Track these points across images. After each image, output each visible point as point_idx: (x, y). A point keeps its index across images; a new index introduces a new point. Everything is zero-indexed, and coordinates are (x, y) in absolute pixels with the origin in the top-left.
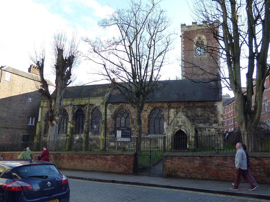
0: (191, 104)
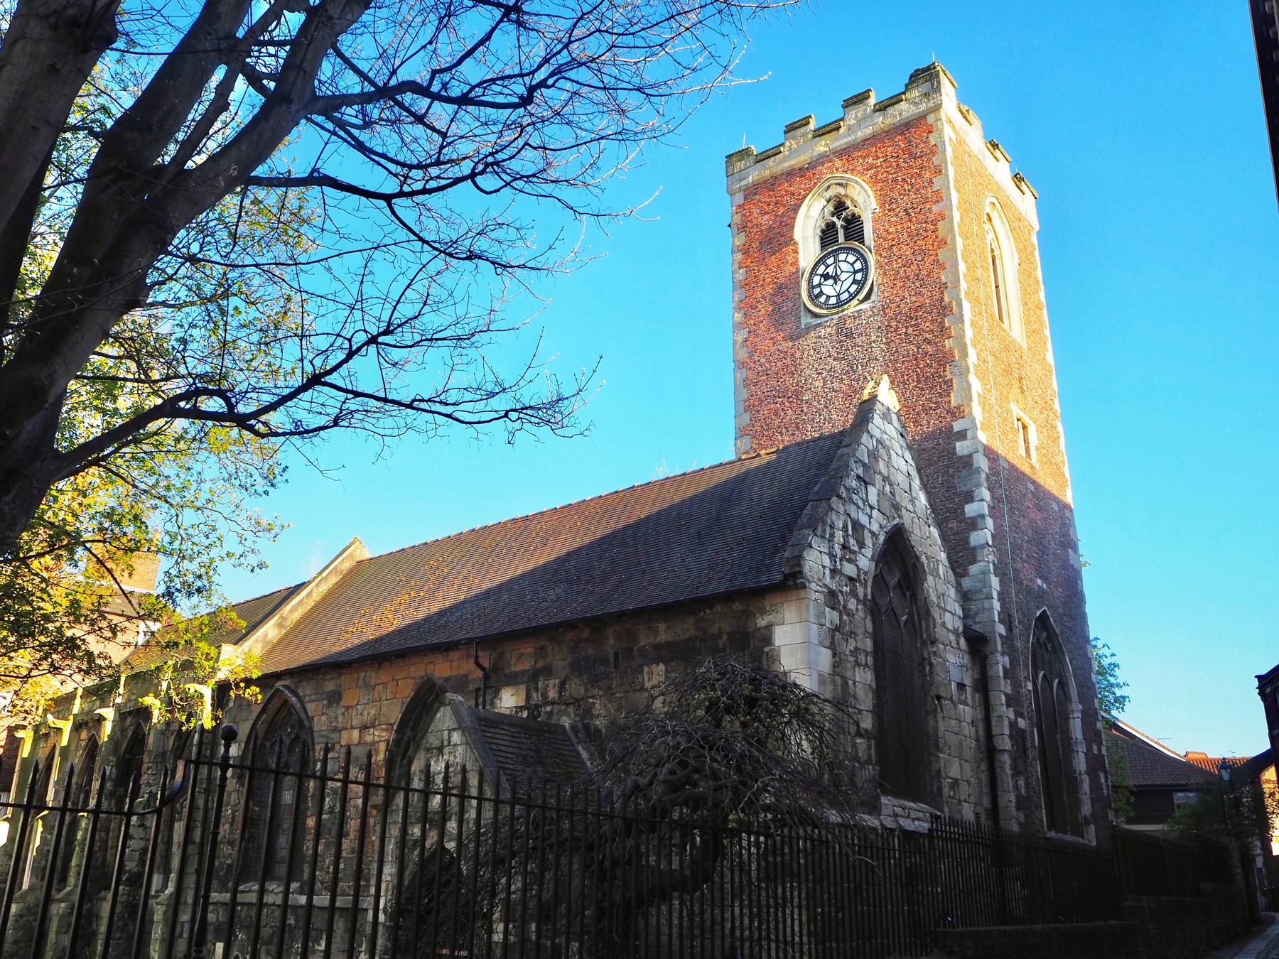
0: (612, 641)
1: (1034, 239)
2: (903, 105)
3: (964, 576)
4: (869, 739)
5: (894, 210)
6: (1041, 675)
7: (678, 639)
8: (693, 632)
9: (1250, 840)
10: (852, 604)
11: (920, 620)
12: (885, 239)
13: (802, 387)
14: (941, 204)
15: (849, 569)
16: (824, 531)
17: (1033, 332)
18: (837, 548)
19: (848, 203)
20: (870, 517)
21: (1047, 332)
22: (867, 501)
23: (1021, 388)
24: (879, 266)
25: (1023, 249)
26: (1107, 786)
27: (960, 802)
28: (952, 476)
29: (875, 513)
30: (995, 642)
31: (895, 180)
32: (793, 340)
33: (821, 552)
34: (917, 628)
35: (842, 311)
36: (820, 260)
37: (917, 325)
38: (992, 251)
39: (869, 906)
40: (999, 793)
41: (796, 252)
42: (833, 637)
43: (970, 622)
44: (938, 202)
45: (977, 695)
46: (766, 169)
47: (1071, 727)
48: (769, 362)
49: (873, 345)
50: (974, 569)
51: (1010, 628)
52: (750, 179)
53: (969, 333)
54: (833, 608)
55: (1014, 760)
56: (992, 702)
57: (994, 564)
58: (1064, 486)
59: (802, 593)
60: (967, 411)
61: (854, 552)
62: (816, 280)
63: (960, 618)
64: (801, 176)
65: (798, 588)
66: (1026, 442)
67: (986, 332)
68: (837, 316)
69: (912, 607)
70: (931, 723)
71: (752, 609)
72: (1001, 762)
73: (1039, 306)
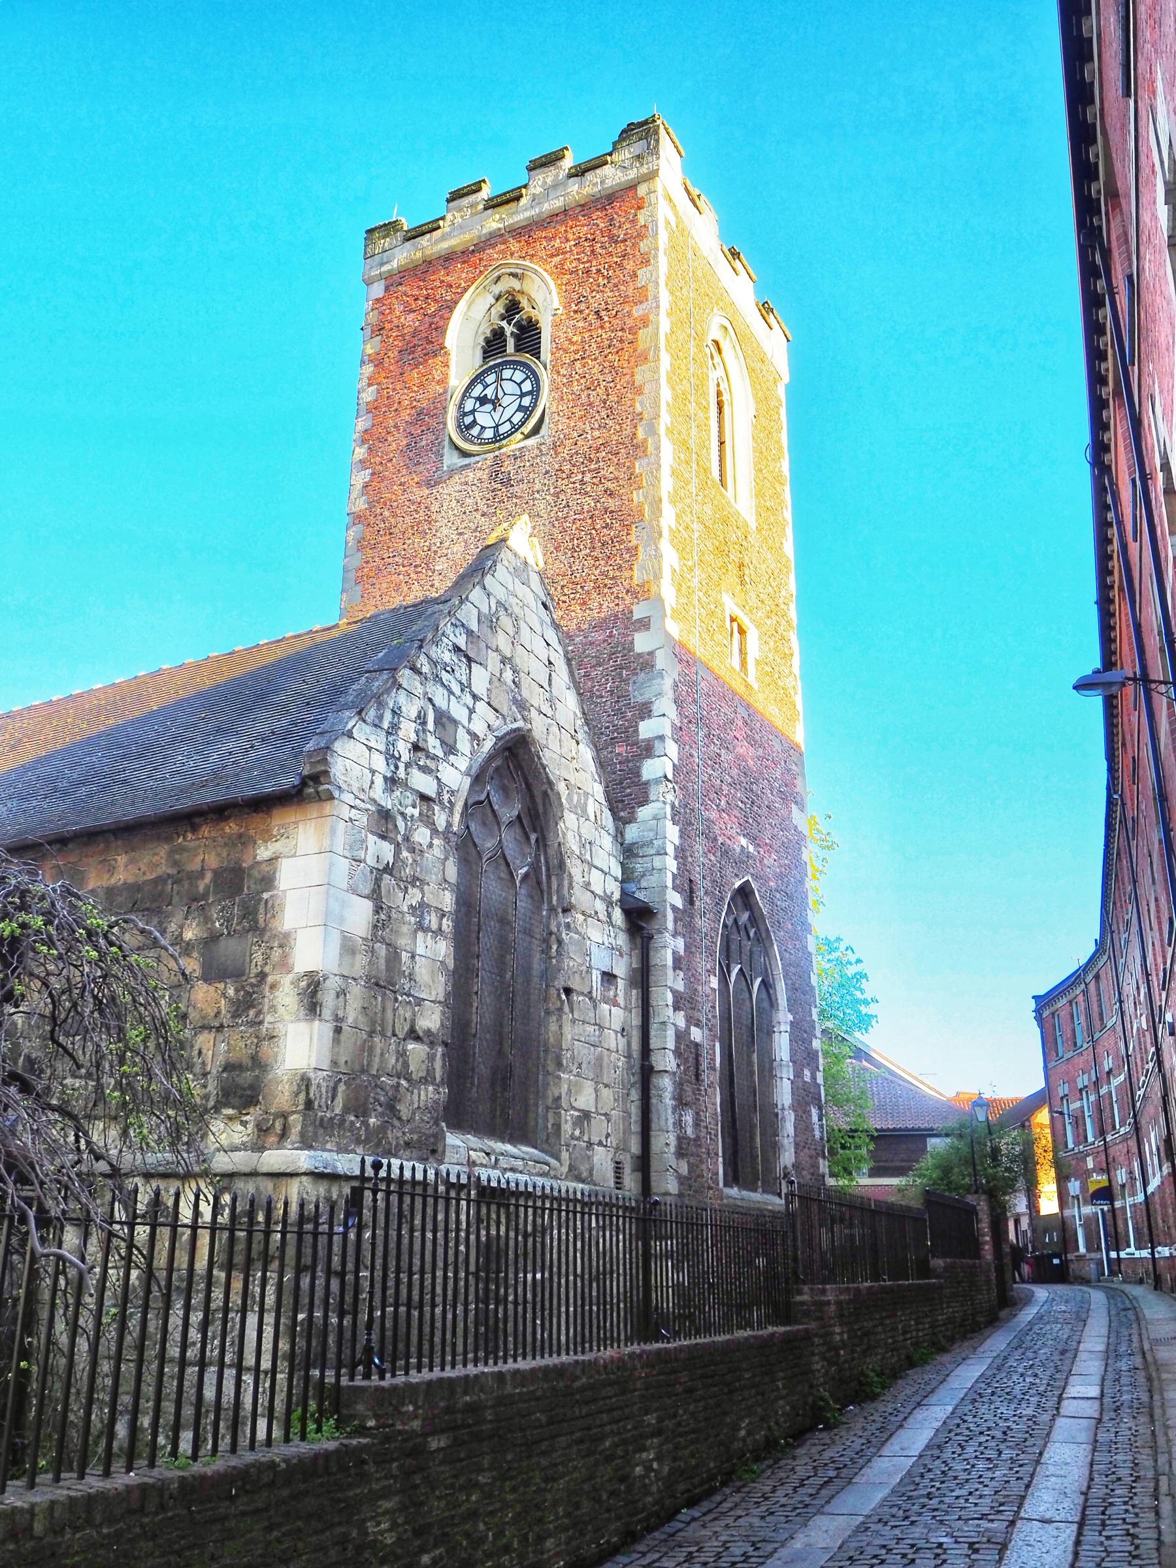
1: (781, 392)
2: (607, 170)
3: (630, 822)
4: (432, 1044)
5: (581, 312)
6: (736, 969)
7: (142, 879)
8: (164, 869)
9: (1007, 1198)
10: (422, 835)
11: (549, 877)
12: (566, 351)
13: (435, 552)
14: (644, 306)
15: (422, 782)
16: (381, 717)
17: (766, 511)
18: (403, 748)
19: (524, 303)
20: (472, 711)
21: (788, 515)
22: (469, 686)
23: (742, 577)
24: (555, 388)
25: (763, 399)
26: (821, 1126)
27: (590, 1144)
28: (626, 681)
29: (481, 707)
30: (665, 916)
31: (587, 272)
32: (429, 485)
33: (370, 748)
34: (545, 886)
35: (500, 448)
36: (477, 377)
37: (597, 471)
38: (719, 394)
39: (396, 1305)
40: (652, 1133)
41: (446, 365)
42: (378, 882)
43: (631, 887)
44: (641, 302)
45: (634, 992)
46: (417, 249)
47: (776, 1045)
48: (395, 516)
49: (537, 495)
50: (644, 813)
51: (690, 900)
52: (395, 264)
53: (667, 484)
54: (383, 837)
55: (679, 1086)
56: (653, 1002)
57: (673, 806)
58: (792, 720)
59: (328, 807)
60: (654, 589)
61: (435, 758)
62: (469, 405)
63: (616, 879)
64: (464, 262)
65: (320, 800)
66: (742, 652)
67: (694, 490)
68: (491, 455)
69: (537, 857)
70: (553, 1027)
71: (252, 832)
72: (659, 1089)
73: (778, 479)
